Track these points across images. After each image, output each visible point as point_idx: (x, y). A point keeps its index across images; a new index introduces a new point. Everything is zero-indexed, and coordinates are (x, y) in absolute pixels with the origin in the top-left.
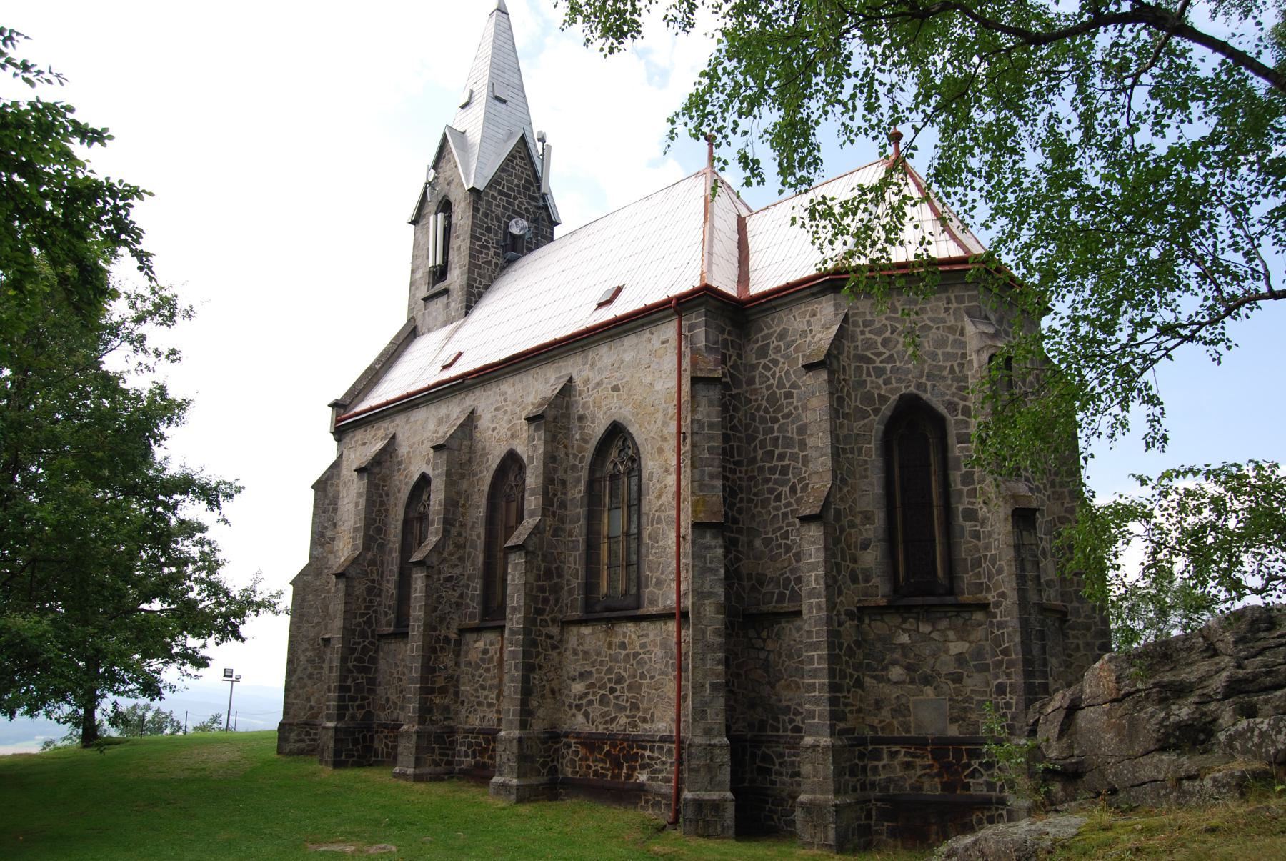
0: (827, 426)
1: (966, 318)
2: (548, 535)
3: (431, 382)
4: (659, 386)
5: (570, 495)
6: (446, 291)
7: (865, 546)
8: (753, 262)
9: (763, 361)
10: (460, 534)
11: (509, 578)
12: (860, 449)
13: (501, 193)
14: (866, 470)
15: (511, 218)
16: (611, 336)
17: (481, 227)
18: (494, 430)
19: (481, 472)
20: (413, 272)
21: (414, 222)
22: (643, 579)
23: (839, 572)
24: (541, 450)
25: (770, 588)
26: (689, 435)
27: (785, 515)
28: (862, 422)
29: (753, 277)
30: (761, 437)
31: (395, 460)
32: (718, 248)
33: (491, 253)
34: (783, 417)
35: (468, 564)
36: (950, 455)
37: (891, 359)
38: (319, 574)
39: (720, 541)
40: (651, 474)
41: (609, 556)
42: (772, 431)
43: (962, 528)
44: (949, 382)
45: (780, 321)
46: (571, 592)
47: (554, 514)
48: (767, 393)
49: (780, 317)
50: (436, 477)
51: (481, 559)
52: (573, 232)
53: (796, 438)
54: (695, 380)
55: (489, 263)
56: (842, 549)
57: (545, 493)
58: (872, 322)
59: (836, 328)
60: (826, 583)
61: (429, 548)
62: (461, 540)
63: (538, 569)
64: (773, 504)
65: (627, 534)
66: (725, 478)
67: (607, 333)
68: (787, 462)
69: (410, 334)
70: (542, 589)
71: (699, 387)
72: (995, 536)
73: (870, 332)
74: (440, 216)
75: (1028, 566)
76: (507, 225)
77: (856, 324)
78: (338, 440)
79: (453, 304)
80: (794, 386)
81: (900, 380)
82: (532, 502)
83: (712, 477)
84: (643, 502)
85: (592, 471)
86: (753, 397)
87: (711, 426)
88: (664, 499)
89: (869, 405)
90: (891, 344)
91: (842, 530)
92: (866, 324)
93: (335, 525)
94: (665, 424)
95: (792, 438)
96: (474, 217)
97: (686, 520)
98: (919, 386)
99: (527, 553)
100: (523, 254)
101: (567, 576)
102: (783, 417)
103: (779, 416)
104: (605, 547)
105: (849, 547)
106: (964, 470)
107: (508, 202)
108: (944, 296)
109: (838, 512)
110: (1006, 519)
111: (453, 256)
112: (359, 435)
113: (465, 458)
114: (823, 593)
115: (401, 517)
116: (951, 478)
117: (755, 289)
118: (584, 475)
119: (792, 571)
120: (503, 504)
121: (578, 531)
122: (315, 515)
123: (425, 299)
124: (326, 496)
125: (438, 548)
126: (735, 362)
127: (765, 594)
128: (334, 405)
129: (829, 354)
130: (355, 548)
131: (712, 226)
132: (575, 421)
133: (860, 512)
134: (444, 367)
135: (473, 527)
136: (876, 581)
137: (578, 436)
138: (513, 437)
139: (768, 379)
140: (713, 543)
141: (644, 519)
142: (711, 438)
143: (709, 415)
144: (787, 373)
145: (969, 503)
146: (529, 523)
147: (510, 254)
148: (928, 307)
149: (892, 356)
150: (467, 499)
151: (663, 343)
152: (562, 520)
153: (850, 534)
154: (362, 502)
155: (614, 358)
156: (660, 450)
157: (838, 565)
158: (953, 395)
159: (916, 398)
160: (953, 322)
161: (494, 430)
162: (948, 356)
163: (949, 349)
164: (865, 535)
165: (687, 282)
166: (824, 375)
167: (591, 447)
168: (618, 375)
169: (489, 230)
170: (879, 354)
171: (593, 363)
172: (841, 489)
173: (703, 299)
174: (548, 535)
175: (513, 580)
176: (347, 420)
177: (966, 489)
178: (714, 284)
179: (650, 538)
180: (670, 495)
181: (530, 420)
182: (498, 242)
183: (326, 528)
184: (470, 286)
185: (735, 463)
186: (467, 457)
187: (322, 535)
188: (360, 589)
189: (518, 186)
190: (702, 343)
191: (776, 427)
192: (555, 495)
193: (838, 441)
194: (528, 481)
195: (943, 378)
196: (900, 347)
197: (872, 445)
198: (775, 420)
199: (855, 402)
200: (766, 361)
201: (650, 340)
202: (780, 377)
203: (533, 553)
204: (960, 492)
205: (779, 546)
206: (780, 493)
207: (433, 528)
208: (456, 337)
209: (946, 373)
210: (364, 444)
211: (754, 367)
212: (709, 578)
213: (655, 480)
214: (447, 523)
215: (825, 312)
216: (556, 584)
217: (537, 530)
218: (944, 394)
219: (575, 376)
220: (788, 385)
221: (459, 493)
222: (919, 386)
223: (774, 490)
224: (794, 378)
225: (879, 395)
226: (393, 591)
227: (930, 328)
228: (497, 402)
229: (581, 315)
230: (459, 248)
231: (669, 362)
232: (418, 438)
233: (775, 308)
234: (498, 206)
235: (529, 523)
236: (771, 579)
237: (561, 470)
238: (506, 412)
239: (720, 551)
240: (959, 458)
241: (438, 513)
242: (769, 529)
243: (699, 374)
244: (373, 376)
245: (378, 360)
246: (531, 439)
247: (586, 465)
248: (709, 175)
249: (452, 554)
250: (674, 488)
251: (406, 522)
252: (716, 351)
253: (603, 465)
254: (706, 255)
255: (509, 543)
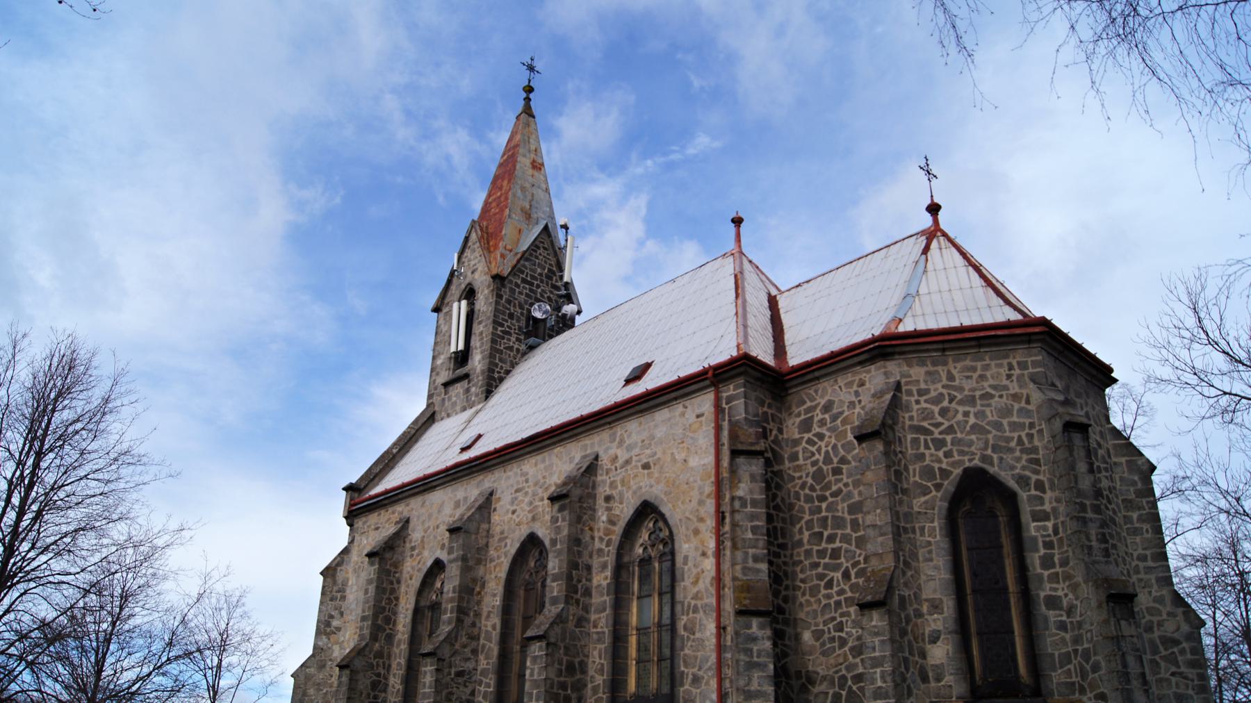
0: (885, 502)
1: (1032, 385)
2: (571, 625)
3: (450, 463)
4: (694, 462)
5: (595, 582)
6: (466, 376)
7: (934, 639)
8: (788, 337)
9: (806, 436)
10: (474, 625)
11: (528, 672)
12: (922, 529)
13: (524, 281)
14: (930, 552)
15: (531, 305)
16: (641, 411)
17: (504, 313)
18: (514, 512)
19: (499, 557)
20: (434, 358)
21: (437, 310)
22: (678, 676)
23: (907, 669)
24: (565, 532)
25: (823, 687)
26: (727, 515)
27: (838, 604)
28: (923, 499)
29: (790, 351)
30: (807, 517)
31: (408, 545)
32: (751, 321)
33: (513, 339)
34: (833, 495)
35: (481, 657)
36: (1025, 535)
37: (950, 430)
38: (322, 666)
39: (768, 632)
40: (686, 558)
41: (639, 650)
42: (819, 510)
43: (1046, 619)
44: (1018, 454)
45: (825, 391)
46: (595, 690)
47: (577, 602)
48: (812, 470)
49: (824, 389)
50: (451, 561)
51: (495, 652)
52: (596, 317)
53: (848, 517)
54: (735, 453)
55: (511, 348)
56: (909, 642)
57: (569, 578)
58: (927, 391)
59: (888, 397)
60: (894, 681)
61: (441, 638)
62: (476, 631)
63: (560, 663)
64: (823, 592)
65: (660, 625)
66: (770, 563)
67: (638, 408)
68: (837, 544)
69: (427, 420)
70: (563, 686)
71: (741, 460)
72: (1087, 626)
73: (926, 401)
74: (464, 303)
75: (1131, 660)
76: (529, 311)
77: (910, 393)
78: (351, 525)
79: (473, 389)
80: (843, 461)
81: (961, 453)
82: (555, 589)
83: (756, 559)
84: (677, 589)
85: (619, 555)
86: (797, 475)
87: (754, 503)
88: (701, 586)
89: (929, 480)
90: (951, 414)
91: (908, 621)
92: (921, 393)
93: (342, 614)
94: (701, 503)
95: (843, 519)
96: (497, 303)
97: (728, 607)
98: (985, 458)
99: (548, 645)
100: (545, 340)
101: (591, 672)
102: (833, 495)
103: (827, 494)
104: (633, 640)
105: (916, 639)
106: (1042, 551)
107: (531, 290)
108: (1005, 362)
109: (902, 599)
110: (1100, 606)
111: (475, 342)
112: (373, 519)
113: (482, 542)
114: (891, 692)
115: (411, 606)
116: (1028, 561)
117: (796, 357)
118: (610, 559)
119: (848, 669)
120: (522, 593)
121: (601, 621)
122: (322, 603)
123: (446, 385)
124: (335, 582)
125: (451, 639)
126: (776, 436)
127: (816, 695)
128: (349, 489)
129: (883, 424)
130: (362, 637)
131: (744, 301)
132: (600, 502)
133: (926, 600)
134: (463, 450)
135: (488, 617)
136: (949, 679)
137: (604, 518)
138: (534, 519)
139: (813, 454)
140: (760, 633)
141: (678, 608)
142: (753, 517)
143: (751, 492)
144: (835, 447)
145: (1051, 589)
146: (551, 611)
147: (532, 340)
148: (988, 374)
149: (951, 427)
150: (483, 586)
151: (698, 416)
152: (586, 609)
153: (916, 625)
154: (372, 588)
155: (645, 435)
156: (696, 532)
157: (906, 660)
158: (1023, 468)
159: (982, 472)
160: (1017, 390)
161: (514, 512)
162: (1015, 426)
163: (1015, 419)
164: (933, 626)
165: (725, 351)
166: (879, 446)
167: (619, 529)
168: (648, 452)
169: (511, 316)
170: (937, 425)
171: (622, 442)
172: (904, 573)
173: (742, 369)
174: (571, 625)
175: (532, 674)
176: (361, 503)
177: (1046, 573)
178: (754, 354)
179: (685, 628)
180: (708, 580)
181: (553, 499)
182: (520, 328)
183: (332, 617)
184: (491, 370)
185: (780, 546)
186: (484, 541)
187: (328, 624)
188: (364, 682)
189: (541, 275)
190: (740, 415)
191: (824, 505)
192: (579, 581)
193: (898, 519)
194: (550, 565)
195: (1011, 450)
196: (960, 417)
197: (936, 524)
198: (822, 499)
199: (914, 476)
200: (810, 435)
201: (683, 414)
202: (827, 452)
203: (555, 644)
204: (1040, 577)
205: (832, 639)
206: (832, 579)
207: (445, 617)
208: (475, 421)
209: (1013, 444)
210: (377, 529)
211: (796, 442)
212: (756, 674)
213: (690, 564)
214: (461, 611)
215: (876, 381)
216: (579, 680)
217: (560, 619)
218: (1013, 468)
219: (601, 454)
220: (835, 460)
221: (474, 581)
222: (985, 458)
223: (824, 576)
224: (842, 452)
225: (940, 469)
226: (399, 687)
227: (992, 396)
228: (518, 483)
229: (611, 390)
230: (481, 333)
231: (705, 438)
232: (431, 524)
233: (818, 378)
234: (520, 293)
235: (551, 611)
236: (824, 678)
237: (586, 553)
238: (526, 493)
239: (768, 645)
240: (1035, 539)
241: (452, 600)
242: (820, 620)
243: (740, 447)
244: (388, 461)
245: (395, 444)
246: (554, 520)
247: (613, 549)
248: (737, 255)
249: (465, 646)
250: (713, 573)
251: (417, 611)
252: (758, 424)
253: (632, 549)
254: (741, 328)
255: (529, 633)
